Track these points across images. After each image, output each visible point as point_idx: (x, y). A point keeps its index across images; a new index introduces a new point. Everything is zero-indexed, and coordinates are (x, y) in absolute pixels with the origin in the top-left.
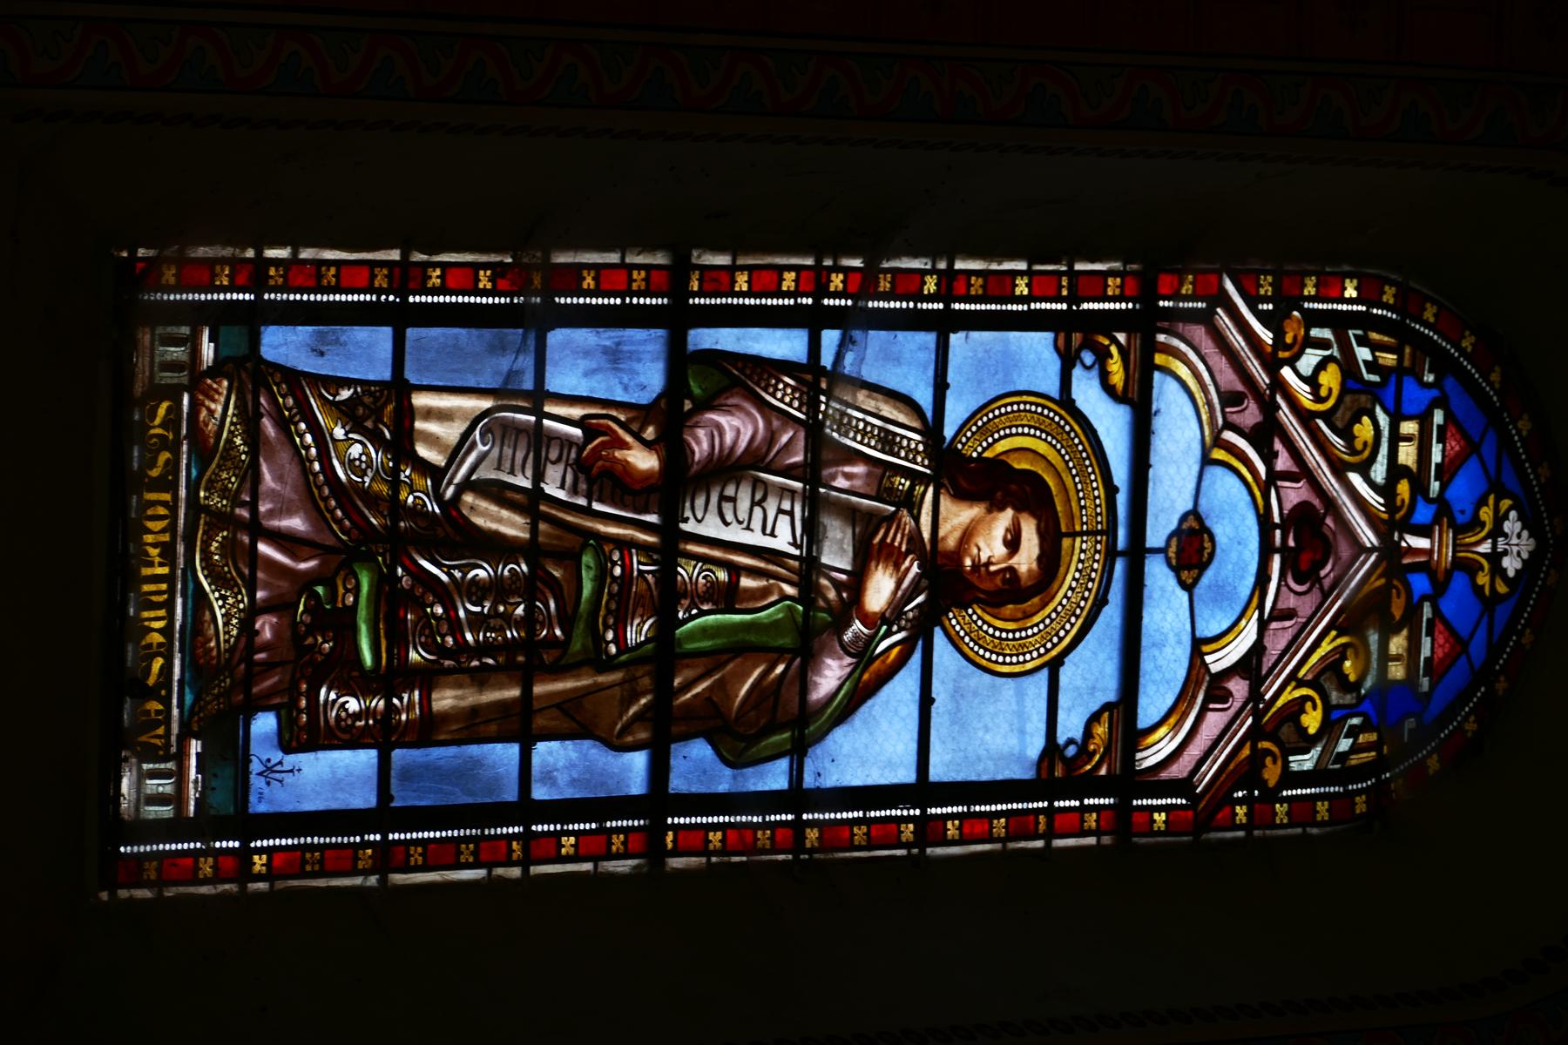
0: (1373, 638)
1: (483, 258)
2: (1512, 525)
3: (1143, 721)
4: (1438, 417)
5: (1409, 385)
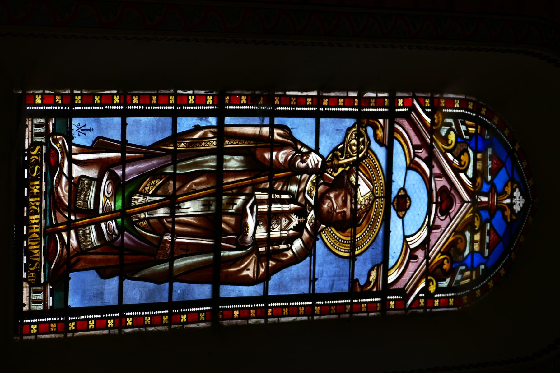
0: (468, 234)
1: (458, 97)
2: (517, 194)
3: (390, 266)
4: (490, 152)
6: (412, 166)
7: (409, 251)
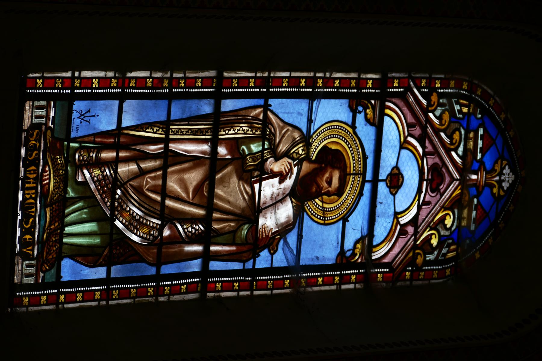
2: (507, 171)
4: (481, 132)
5: (472, 118)
6: (404, 145)
7: (399, 227)
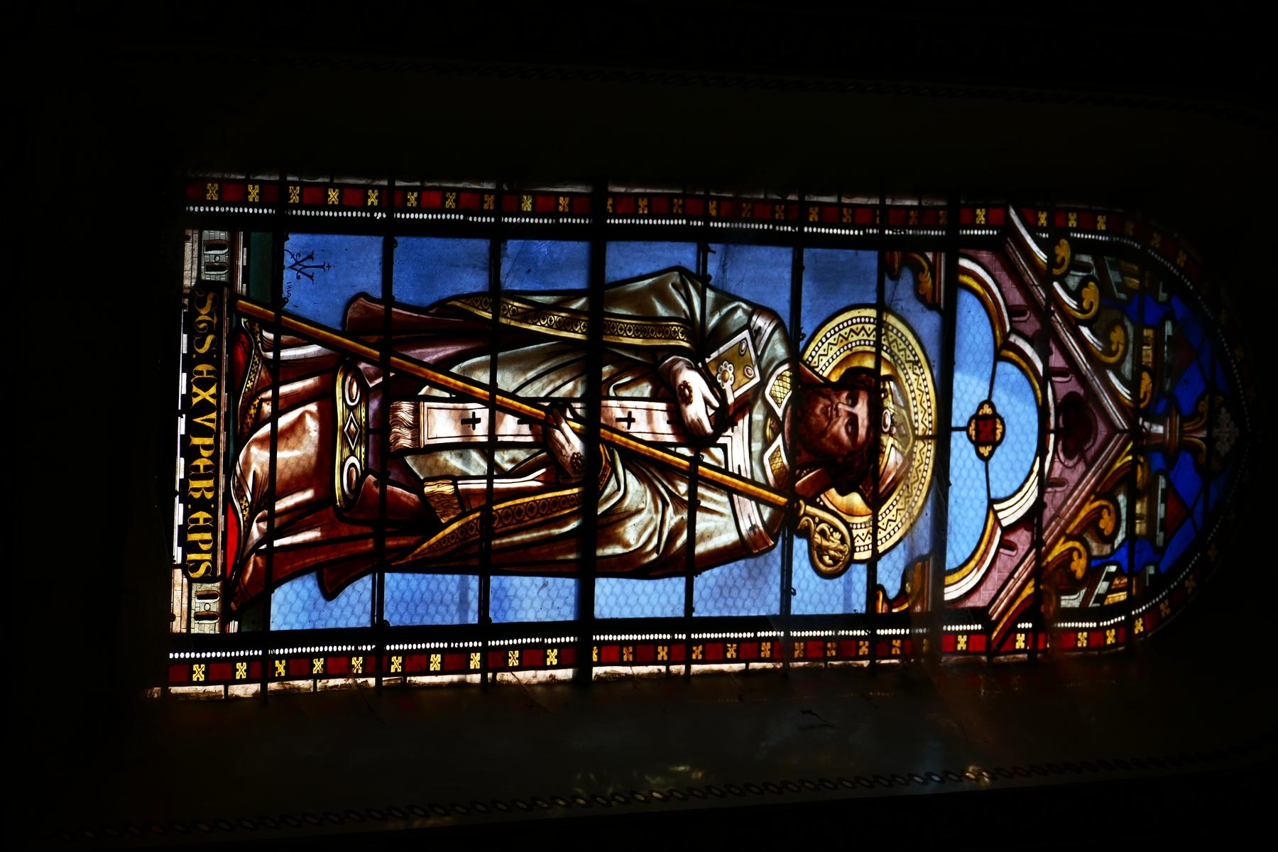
0: (1122, 499)
2: (1224, 415)
3: (951, 563)
7: (999, 532)
